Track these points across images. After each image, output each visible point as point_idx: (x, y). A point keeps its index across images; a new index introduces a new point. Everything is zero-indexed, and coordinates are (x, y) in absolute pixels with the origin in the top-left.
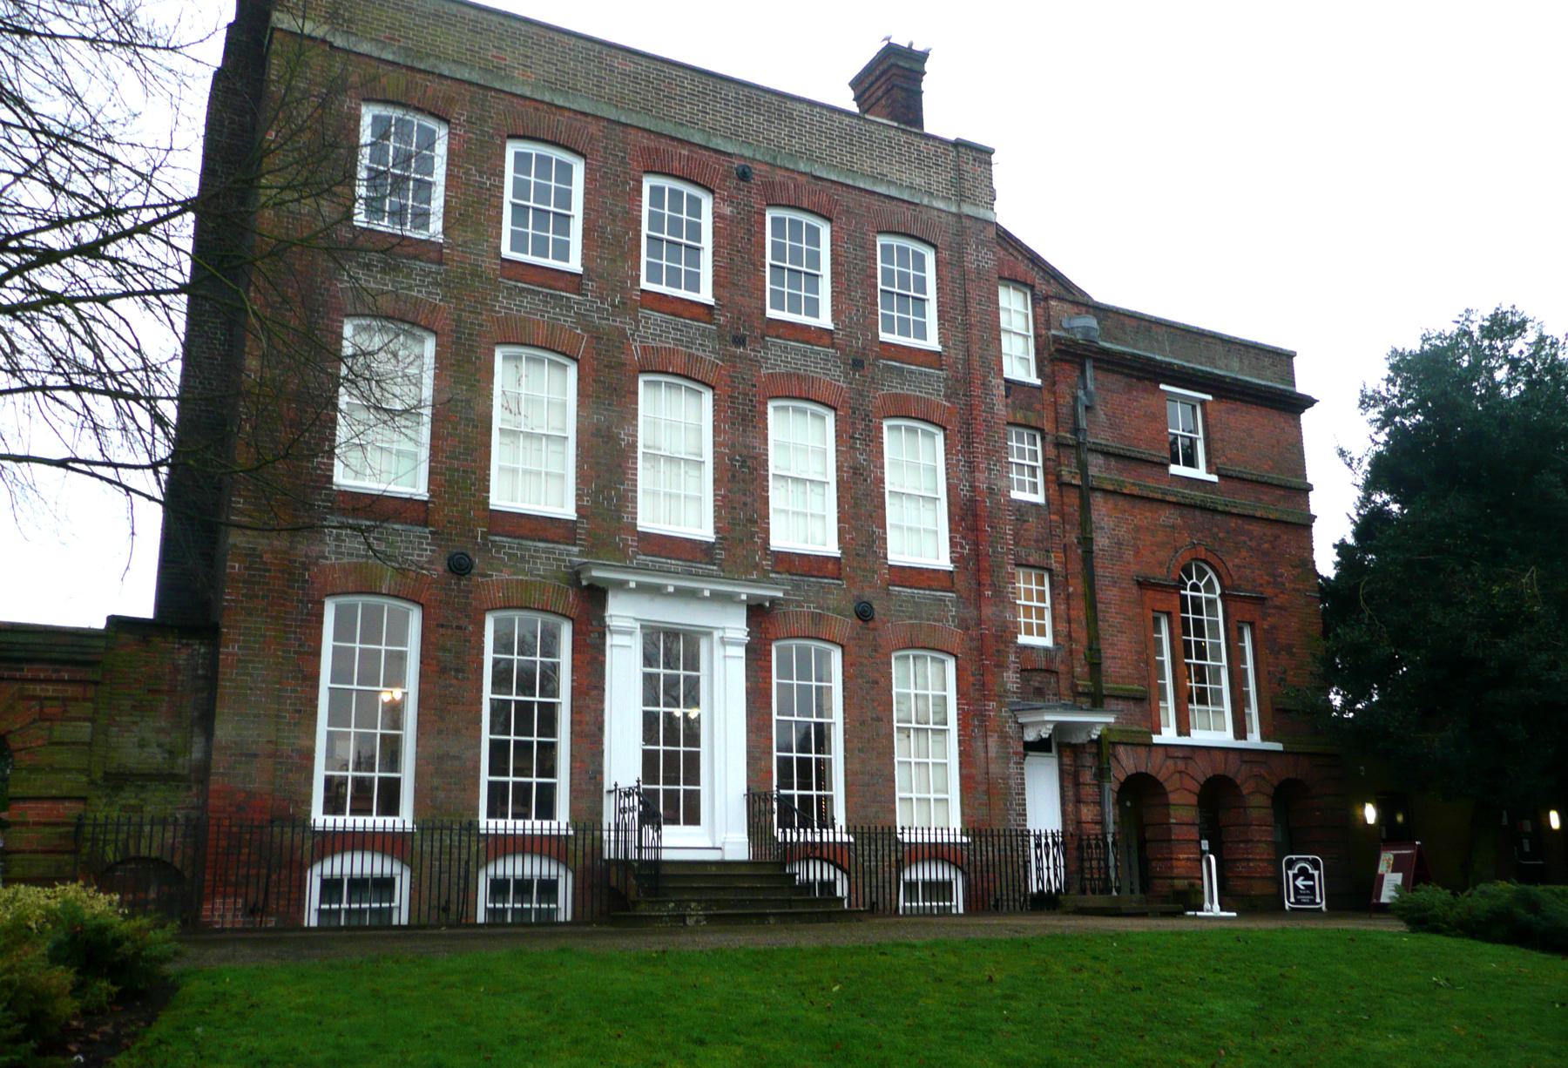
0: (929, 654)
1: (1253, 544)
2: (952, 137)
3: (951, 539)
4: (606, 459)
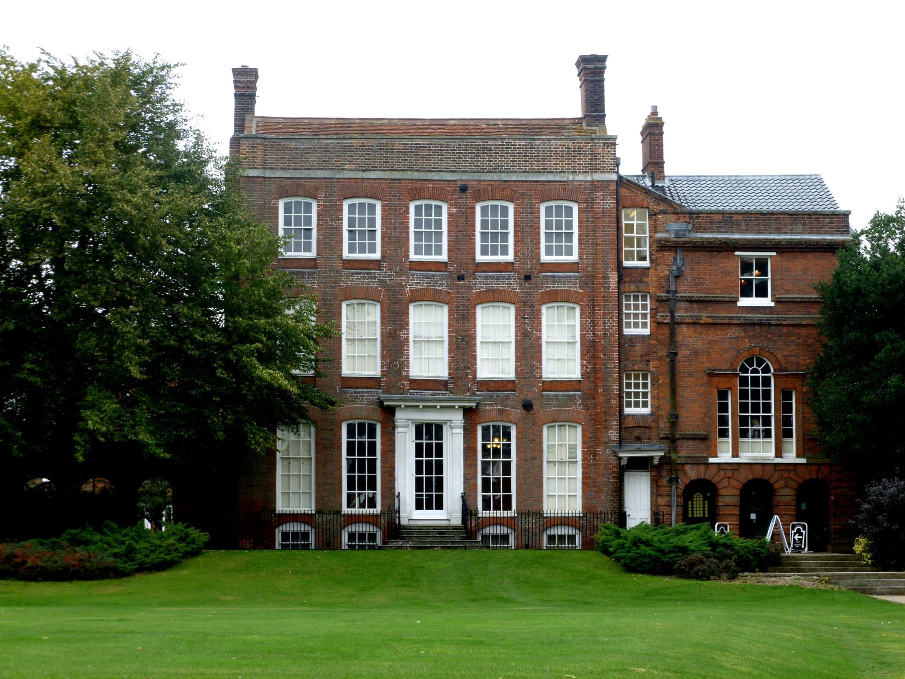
0: (567, 424)
1: (801, 341)
4: (394, 345)
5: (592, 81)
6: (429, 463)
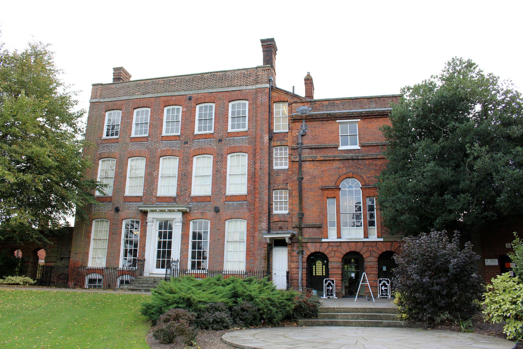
2: (255, 66)
3: (226, 187)
4: (151, 179)
5: (266, 51)
6: (165, 242)
